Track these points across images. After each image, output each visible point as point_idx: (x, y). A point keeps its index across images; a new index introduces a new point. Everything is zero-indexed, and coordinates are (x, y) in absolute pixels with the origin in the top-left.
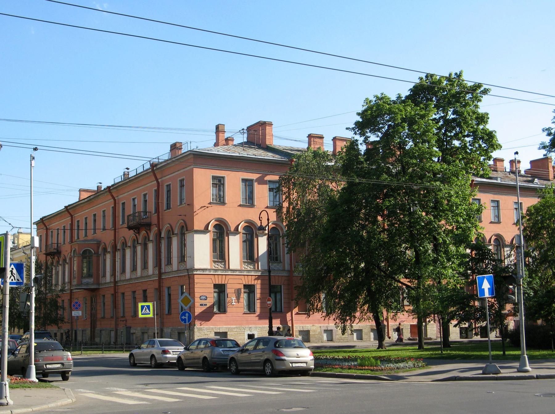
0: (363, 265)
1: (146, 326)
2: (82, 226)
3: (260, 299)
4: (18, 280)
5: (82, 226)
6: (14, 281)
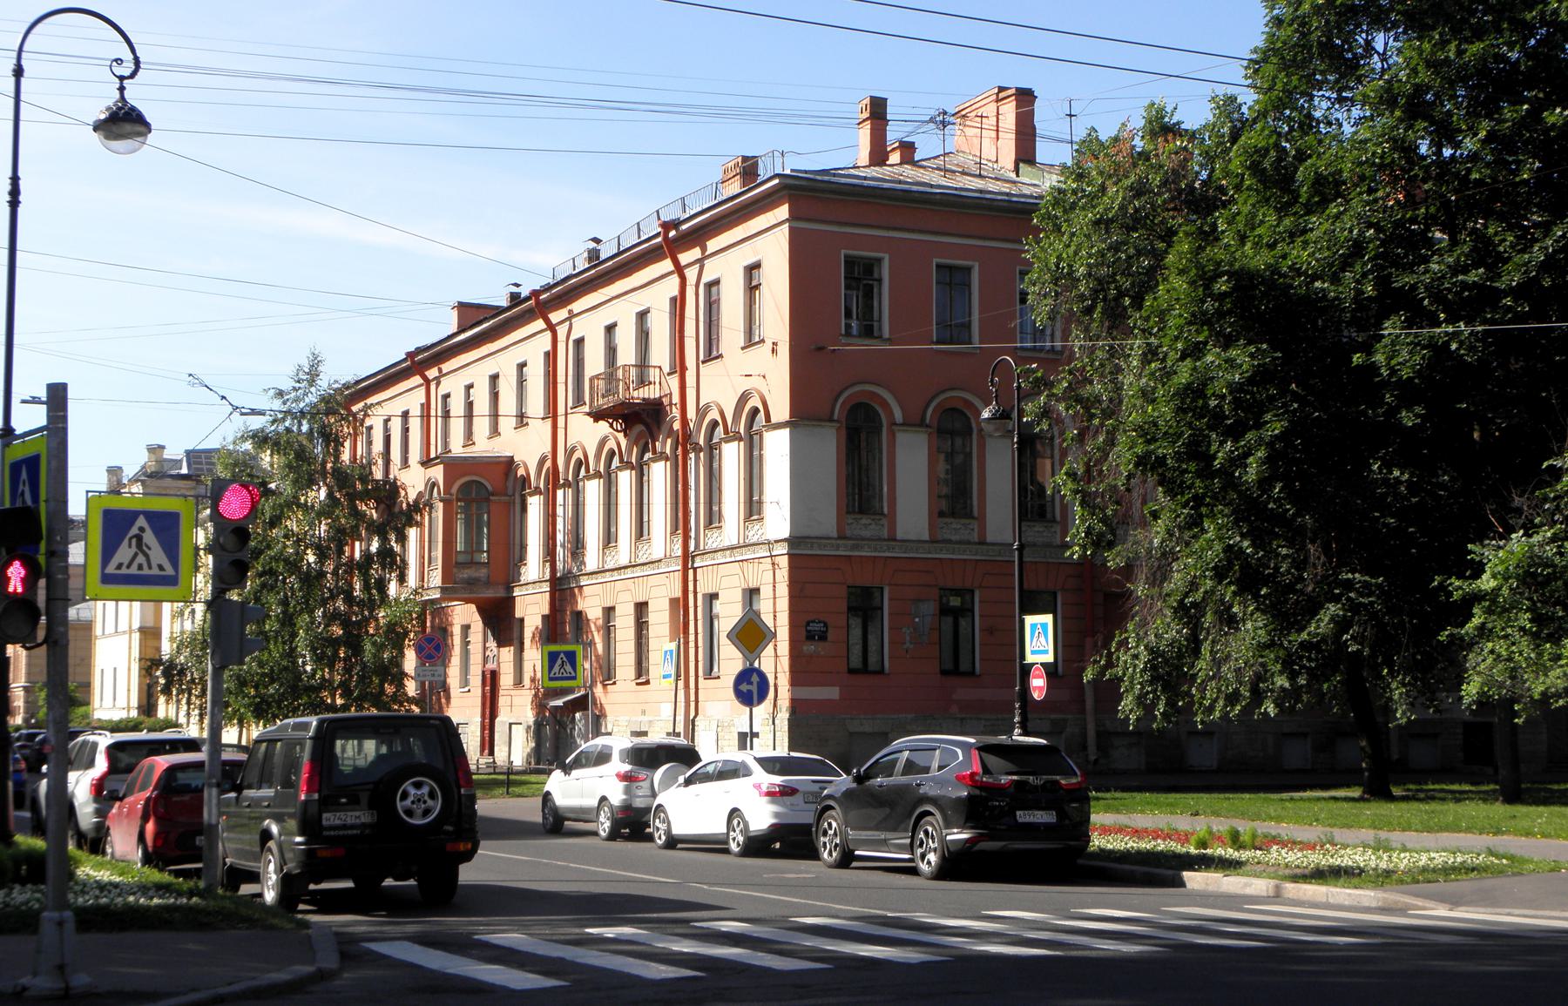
0: (1476, 435)
1: (644, 712)
2: (457, 407)
3: (206, 602)
4: (161, 567)
5: (457, 407)
6: (146, 571)
